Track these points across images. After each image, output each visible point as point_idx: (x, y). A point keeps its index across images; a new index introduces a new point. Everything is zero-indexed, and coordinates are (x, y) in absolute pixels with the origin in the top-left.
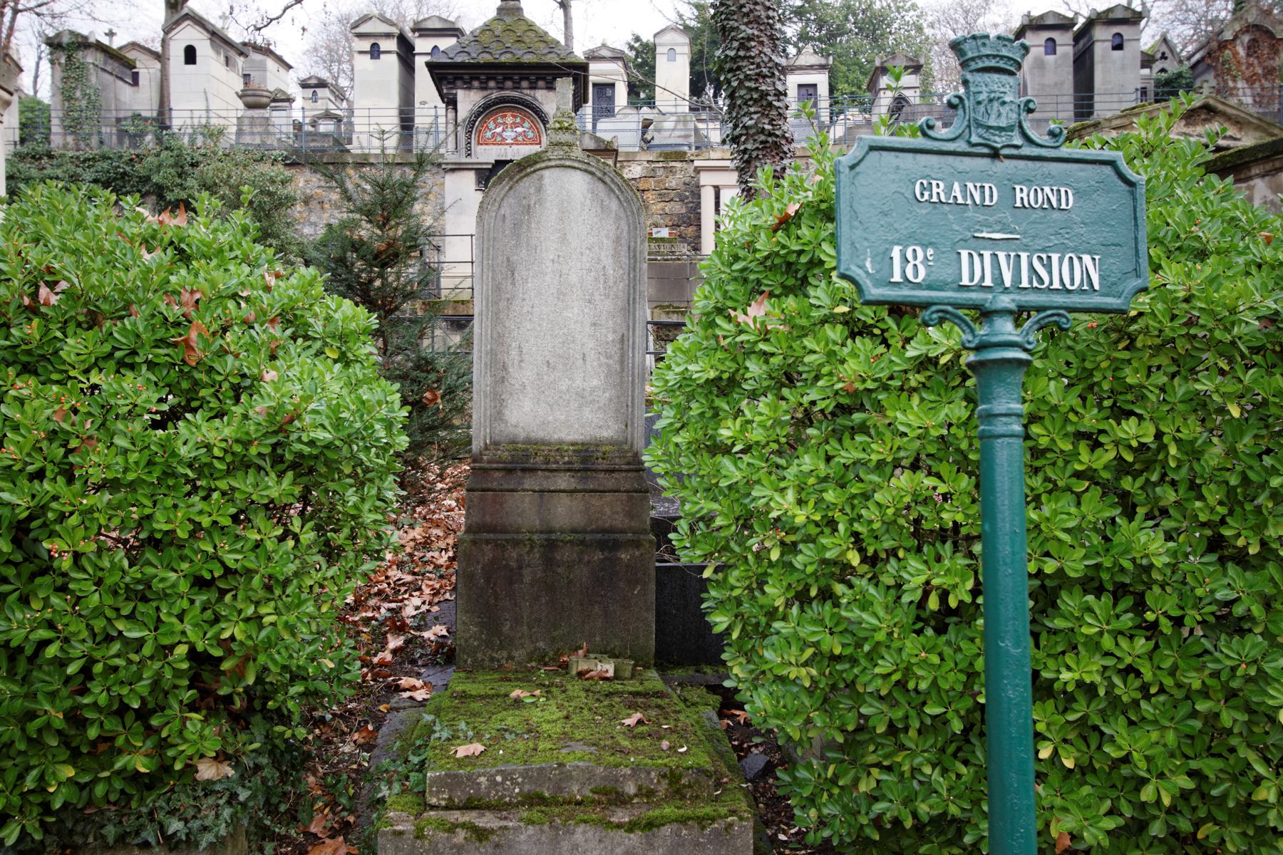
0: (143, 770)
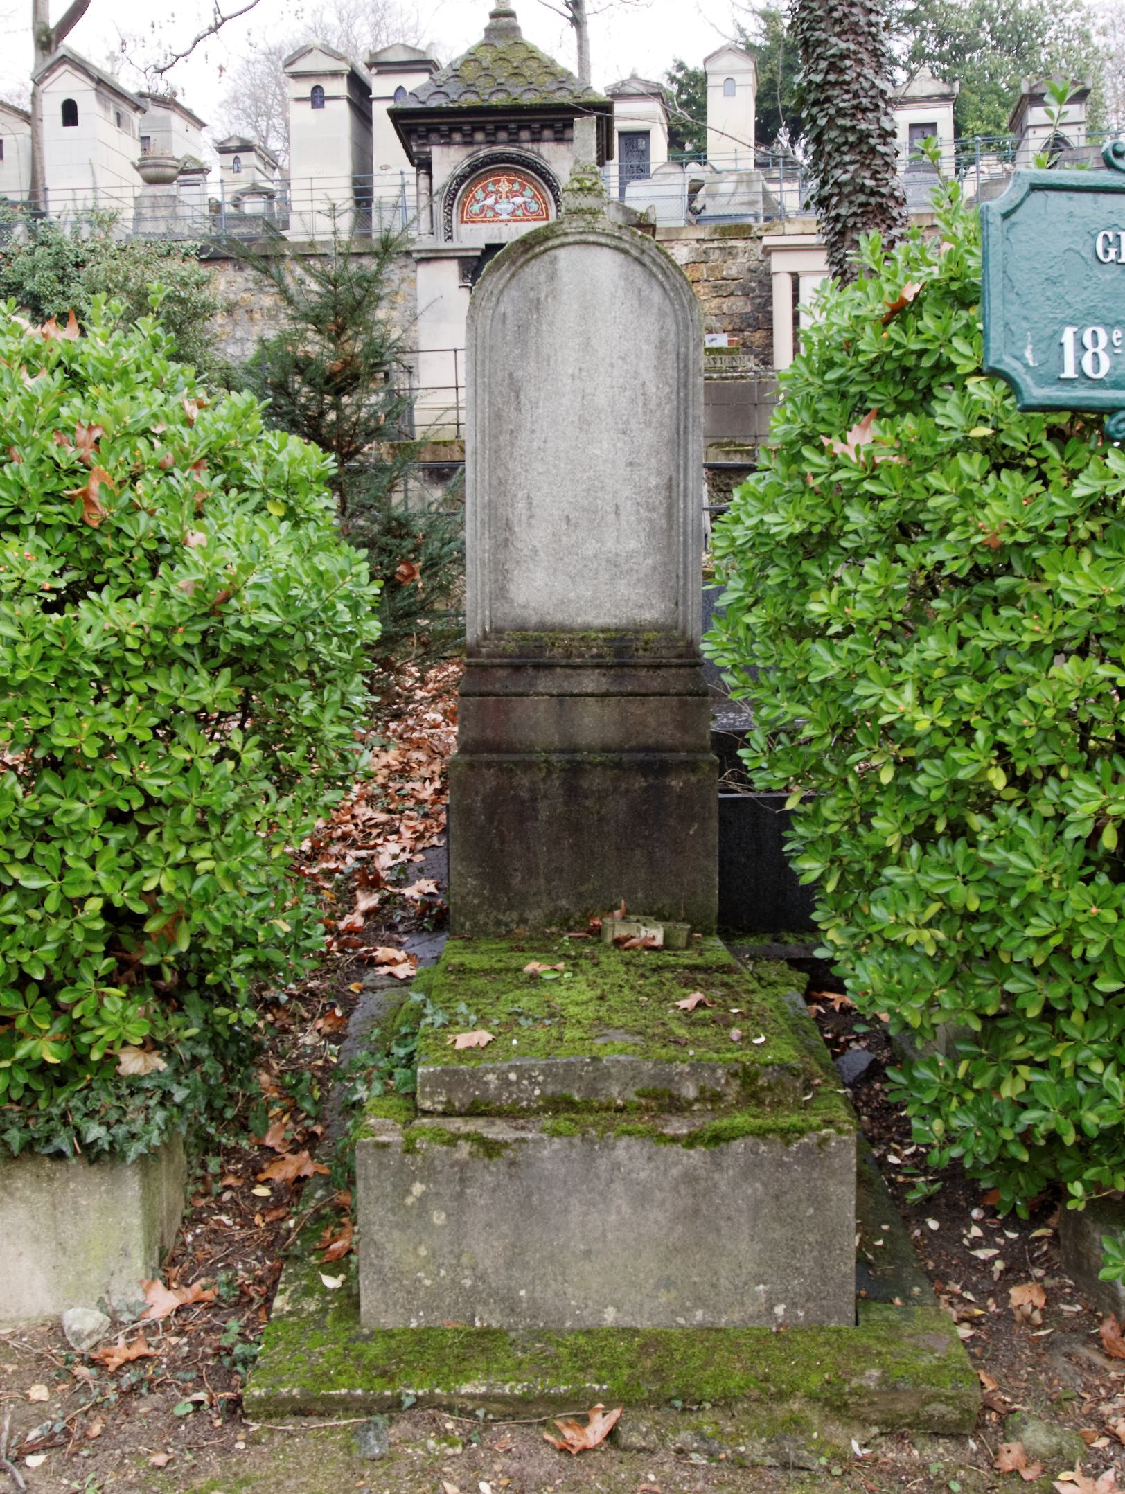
0: (52, 1060)
